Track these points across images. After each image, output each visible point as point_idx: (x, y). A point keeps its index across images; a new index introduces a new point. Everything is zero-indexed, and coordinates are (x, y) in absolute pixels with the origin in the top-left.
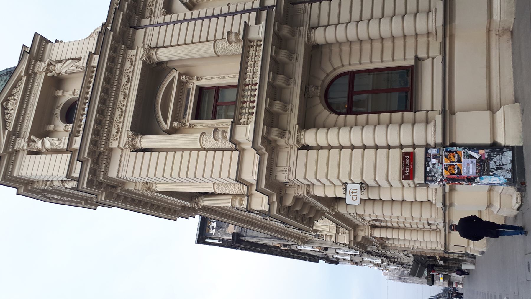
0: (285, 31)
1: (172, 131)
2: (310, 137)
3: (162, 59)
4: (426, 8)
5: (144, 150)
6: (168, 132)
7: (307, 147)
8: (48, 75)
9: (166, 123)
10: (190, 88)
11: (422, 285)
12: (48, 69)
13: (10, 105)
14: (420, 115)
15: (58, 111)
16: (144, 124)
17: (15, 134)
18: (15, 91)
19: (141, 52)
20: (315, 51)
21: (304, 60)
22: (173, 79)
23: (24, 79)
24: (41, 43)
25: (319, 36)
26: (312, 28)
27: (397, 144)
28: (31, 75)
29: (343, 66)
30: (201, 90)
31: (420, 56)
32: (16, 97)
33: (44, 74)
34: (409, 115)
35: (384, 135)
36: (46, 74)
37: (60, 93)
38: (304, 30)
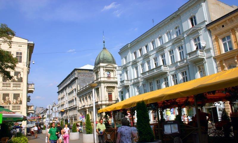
16: (108, 87)
17: (106, 67)
28: (114, 68)
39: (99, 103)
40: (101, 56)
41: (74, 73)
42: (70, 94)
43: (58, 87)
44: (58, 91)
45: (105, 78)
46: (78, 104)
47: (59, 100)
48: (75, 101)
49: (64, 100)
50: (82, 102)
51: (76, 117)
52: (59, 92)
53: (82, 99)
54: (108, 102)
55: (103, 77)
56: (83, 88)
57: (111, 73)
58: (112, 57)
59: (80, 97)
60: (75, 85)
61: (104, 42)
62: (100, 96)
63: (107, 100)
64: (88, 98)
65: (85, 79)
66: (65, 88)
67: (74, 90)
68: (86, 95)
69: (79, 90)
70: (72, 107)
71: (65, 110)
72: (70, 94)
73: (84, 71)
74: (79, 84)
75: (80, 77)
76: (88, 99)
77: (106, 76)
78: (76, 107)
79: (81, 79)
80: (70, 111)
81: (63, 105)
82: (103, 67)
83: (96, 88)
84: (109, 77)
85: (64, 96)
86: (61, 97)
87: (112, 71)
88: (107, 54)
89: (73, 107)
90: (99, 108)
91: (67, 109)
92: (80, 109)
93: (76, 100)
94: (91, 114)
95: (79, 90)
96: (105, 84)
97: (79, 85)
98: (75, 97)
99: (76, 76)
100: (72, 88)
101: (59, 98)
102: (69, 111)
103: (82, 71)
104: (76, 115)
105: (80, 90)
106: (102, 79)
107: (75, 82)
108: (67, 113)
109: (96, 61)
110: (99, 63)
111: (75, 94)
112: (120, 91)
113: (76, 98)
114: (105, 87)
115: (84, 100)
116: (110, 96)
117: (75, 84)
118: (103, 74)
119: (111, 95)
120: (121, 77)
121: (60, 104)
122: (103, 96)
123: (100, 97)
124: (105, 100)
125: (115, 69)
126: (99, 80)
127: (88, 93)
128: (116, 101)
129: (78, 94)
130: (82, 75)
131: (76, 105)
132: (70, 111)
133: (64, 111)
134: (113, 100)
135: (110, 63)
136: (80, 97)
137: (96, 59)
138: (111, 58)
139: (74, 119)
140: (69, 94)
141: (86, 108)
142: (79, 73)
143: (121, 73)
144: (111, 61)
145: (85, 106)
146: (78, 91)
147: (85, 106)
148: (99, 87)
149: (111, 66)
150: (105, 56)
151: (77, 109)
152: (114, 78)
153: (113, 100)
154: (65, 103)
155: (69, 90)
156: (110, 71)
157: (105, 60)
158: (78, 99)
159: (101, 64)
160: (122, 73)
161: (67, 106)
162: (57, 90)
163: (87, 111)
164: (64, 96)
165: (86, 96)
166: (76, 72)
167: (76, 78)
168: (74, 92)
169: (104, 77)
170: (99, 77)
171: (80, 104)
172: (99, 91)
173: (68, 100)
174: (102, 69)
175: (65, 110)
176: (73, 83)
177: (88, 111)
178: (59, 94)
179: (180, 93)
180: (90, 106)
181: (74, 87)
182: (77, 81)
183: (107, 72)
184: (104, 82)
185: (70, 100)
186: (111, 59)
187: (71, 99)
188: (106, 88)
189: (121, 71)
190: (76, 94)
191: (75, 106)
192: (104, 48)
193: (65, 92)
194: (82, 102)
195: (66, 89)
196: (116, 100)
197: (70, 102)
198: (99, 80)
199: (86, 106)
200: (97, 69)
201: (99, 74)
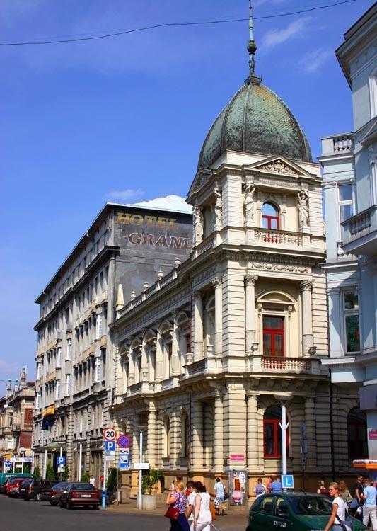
0: (314, 385)
1: (257, 303)
2: (253, 402)
3: (304, 293)
4: (318, 458)
5: (245, 287)
6: (256, 300)
7: (246, 400)
8: (299, 194)
9: (262, 298)
11: (221, 128)
12: (302, 194)
13: (278, 166)
14: (262, 461)
16: (263, 284)
17: (257, 175)
18: (288, 169)
19: (308, 279)
22: (290, 301)
23: (297, 176)
25: (309, 404)
26: (315, 401)
27: (245, 447)
28: (300, 181)
29: (292, 417)
30: (283, 318)
31: (294, 460)
32: (283, 170)
33: (299, 190)
34: (262, 455)
35: (254, 450)
36: (299, 192)
38: (313, 395)
39: (213, 368)
40: (235, 118)
41: (102, 231)
42: (83, 329)
43: (39, 305)
44: (36, 320)
45: (251, 234)
46: (112, 377)
47: (40, 360)
48: (40, 396)
49: (58, 361)
50: (133, 367)
51: (101, 444)
52: (40, 328)
53: (162, 342)
54: (258, 366)
55: (241, 225)
56: (139, 297)
57: (283, 207)
58: (294, 123)
59: (123, 346)
60: (106, 286)
61: (251, 8)
62: (219, 327)
63: (256, 353)
64: (174, 335)
65: (153, 259)
66: (63, 308)
67: (99, 311)
68: (149, 332)
69: (120, 308)
70: (87, 391)
71: (58, 405)
72: (83, 329)
73: (150, 220)
74: (122, 280)
75: (129, 249)
76: (161, 354)
77: (257, 221)
78: (104, 393)
79: (133, 259)
80: (79, 413)
81: (51, 385)
82: (242, 172)
83: (200, 291)
84: (272, 229)
85: (59, 341)
86: (47, 349)
87: (293, 197)
88: (266, 108)
89: (91, 393)
90: (208, 395)
91: (67, 402)
92: (119, 401)
93: (104, 357)
94: (168, 429)
95: (121, 311)
96: (250, 265)
97: (121, 286)
98: (103, 342)
99: (111, 243)
100: (91, 301)
101: (39, 354)
102: (76, 412)
103: (141, 220)
104: (100, 435)
105: (126, 307)
106: (235, 238)
107: (107, 268)
108: (67, 420)
109: (205, 152)
110: (220, 153)
111: (101, 330)
112: (341, 289)
113: (103, 350)
114: (246, 281)
115: (140, 359)
116: (273, 332)
117: (104, 280)
118: (238, 213)
119: (282, 332)
120: (348, 202)
121: (42, 378)
122: (236, 332)
123: (219, 338)
124: (242, 354)
125: (305, 189)
126: (219, 241)
127: (163, 319)
128: (308, 361)
129: (115, 330)
130: (142, 239)
131: (103, 383)
132: (79, 413)
133: (55, 411)
134: (287, 355)
135: (283, 154)
136: (123, 343)
137: (206, 139)
138: (285, 132)
139: (93, 453)
140: (77, 330)
141: (147, 398)
142: (125, 229)
143: (349, 176)
144: (284, 146)
145: (139, 386)
146: (115, 314)
147: (139, 386)
148: (216, 278)
149: (284, 173)
150: (254, 118)
151: (108, 402)
152: (300, 235)
153: (287, 355)
154: (61, 375)
155: (78, 313)
156: (278, 201)
157: (255, 134)
158: (113, 352)
159: (233, 159)
160: (355, 179)
161: (67, 389)
162: (35, 314)
163: (147, 413)
164: (59, 341)
165: (150, 335)
166: (111, 223)
167: (112, 252)
168: (99, 320)
169: (245, 229)
170: (219, 229)
171: (118, 378)
172: (213, 303)
173: (75, 363)
174: (233, 185)
175: (60, 409)
176: (99, 275)
177: (157, 413)
178: (41, 336)
179: (213, 298)
180: (167, 387)
181: (101, 294)
182: (116, 267)
183: (260, 204)
184: (245, 254)
185: (81, 359)
186: (286, 136)
187: (83, 357)
188: (251, 289)
189: (349, 166)
190: (108, 329)
191: (98, 390)
192: (253, 81)
193: (63, 325)
194: (133, 367)
195: (67, 311)
196: (307, 356)
197: (82, 368)
198: (219, 241)
199: (146, 389)
200: (210, 185)
201: (217, 212)
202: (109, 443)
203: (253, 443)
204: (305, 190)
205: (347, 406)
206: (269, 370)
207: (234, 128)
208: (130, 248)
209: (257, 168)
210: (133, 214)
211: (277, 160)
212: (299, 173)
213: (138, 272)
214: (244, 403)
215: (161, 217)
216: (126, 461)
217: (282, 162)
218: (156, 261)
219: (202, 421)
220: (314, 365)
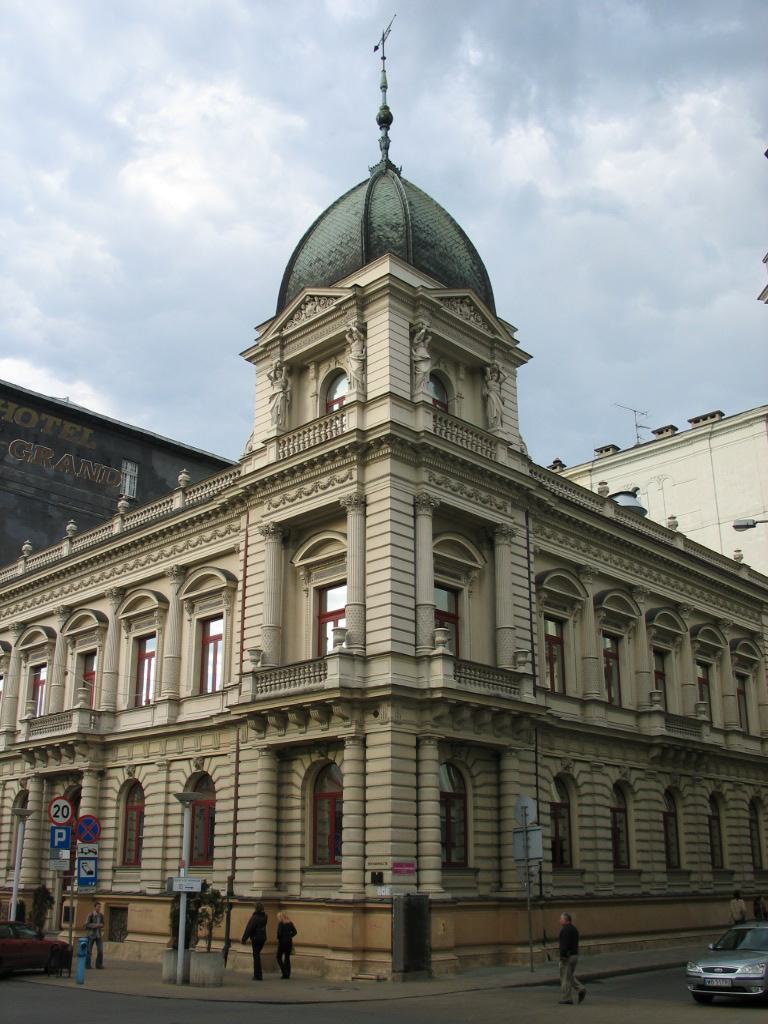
7: (417, 747)
10: (460, 579)
15: (442, 367)
20: (496, 755)
21: (326, 341)
23: (489, 334)
24: (522, 358)
37: (462, 376)
79: (13, 486)
188: (426, 525)
202: (57, 831)
203: (352, 838)
204: (500, 364)
205: (550, 770)
206: (463, 687)
207: (387, 225)
208: (9, 465)
209: (441, 299)
210: (21, 405)
211: (465, 297)
212: (494, 331)
213: (19, 512)
214: (412, 754)
215: (69, 421)
216: (90, 873)
217: (471, 304)
218: (54, 497)
219: (275, 791)
220: (105, 722)
